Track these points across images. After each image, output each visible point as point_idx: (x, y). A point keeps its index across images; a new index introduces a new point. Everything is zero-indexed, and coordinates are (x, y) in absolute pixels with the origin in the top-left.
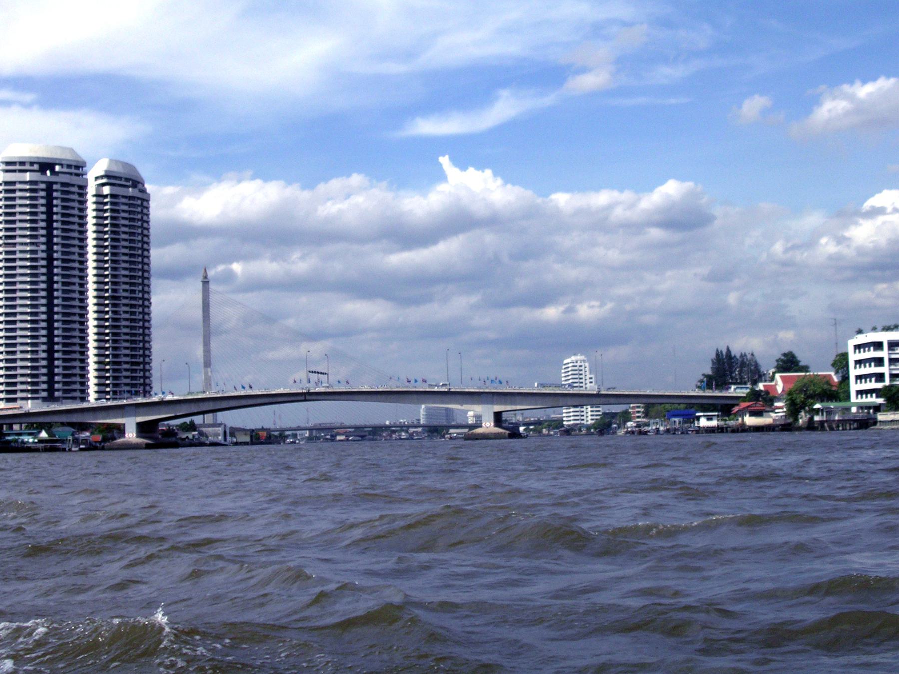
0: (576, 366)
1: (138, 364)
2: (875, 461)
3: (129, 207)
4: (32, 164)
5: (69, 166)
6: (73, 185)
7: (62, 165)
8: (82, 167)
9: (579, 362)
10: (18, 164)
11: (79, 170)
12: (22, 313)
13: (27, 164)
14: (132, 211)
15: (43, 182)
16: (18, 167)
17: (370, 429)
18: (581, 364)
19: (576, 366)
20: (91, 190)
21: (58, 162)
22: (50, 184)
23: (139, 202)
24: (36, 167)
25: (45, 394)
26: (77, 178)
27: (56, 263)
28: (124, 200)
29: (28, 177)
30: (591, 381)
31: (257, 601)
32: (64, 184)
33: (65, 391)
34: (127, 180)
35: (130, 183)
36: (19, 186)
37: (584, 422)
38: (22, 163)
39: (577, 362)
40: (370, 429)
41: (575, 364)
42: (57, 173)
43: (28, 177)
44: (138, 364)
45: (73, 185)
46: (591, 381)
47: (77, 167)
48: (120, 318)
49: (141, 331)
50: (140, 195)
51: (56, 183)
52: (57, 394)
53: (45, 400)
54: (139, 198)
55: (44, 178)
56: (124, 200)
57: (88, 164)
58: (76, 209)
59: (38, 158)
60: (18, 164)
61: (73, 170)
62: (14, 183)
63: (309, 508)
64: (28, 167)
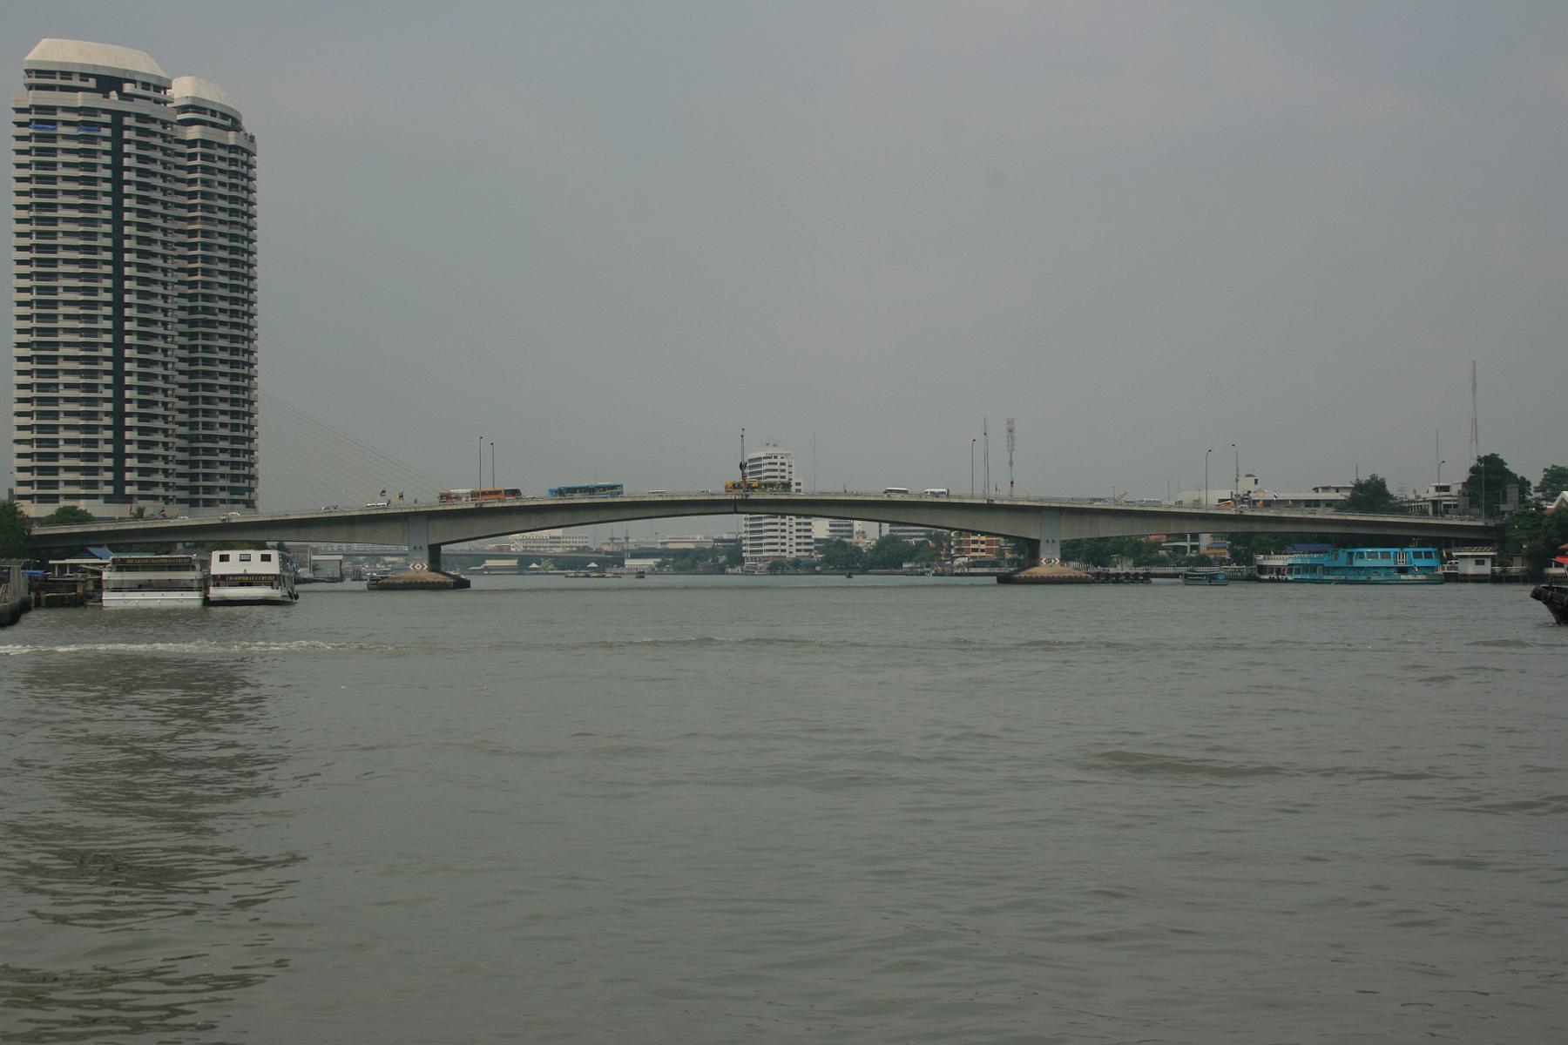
0: (776, 464)
4: (85, 76)
5: (146, 86)
6: (154, 120)
8: (165, 89)
9: (779, 457)
11: (160, 92)
12: (67, 344)
13: (74, 76)
15: (105, 111)
16: (58, 81)
18: (783, 461)
19: (776, 464)
22: (118, 115)
24: (92, 83)
25: (109, 490)
26: (157, 105)
27: (127, 257)
28: (221, 152)
29: (79, 99)
30: (798, 487)
31: (139, 833)
32: (141, 117)
33: (142, 485)
34: (224, 116)
37: (786, 554)
38: (66, 75)
39: (776, 457)
41: (773, 460)
42: (129, 97)
43: (79, 99)
45: (154, 120)
46: (798, 487)
47: (158, 89)
48: (214, 359)
50: (244, 145)
51: (128, 114)
52: (128, 490)
53: (108, 499)
55: (105, 104)
56: (221, 152)
58: (159, 163)
59: (95, 67)
60: (58, 76)
61: (151, 93)
62: (52, 109)
63: (258, 686)
64: (76, 82)
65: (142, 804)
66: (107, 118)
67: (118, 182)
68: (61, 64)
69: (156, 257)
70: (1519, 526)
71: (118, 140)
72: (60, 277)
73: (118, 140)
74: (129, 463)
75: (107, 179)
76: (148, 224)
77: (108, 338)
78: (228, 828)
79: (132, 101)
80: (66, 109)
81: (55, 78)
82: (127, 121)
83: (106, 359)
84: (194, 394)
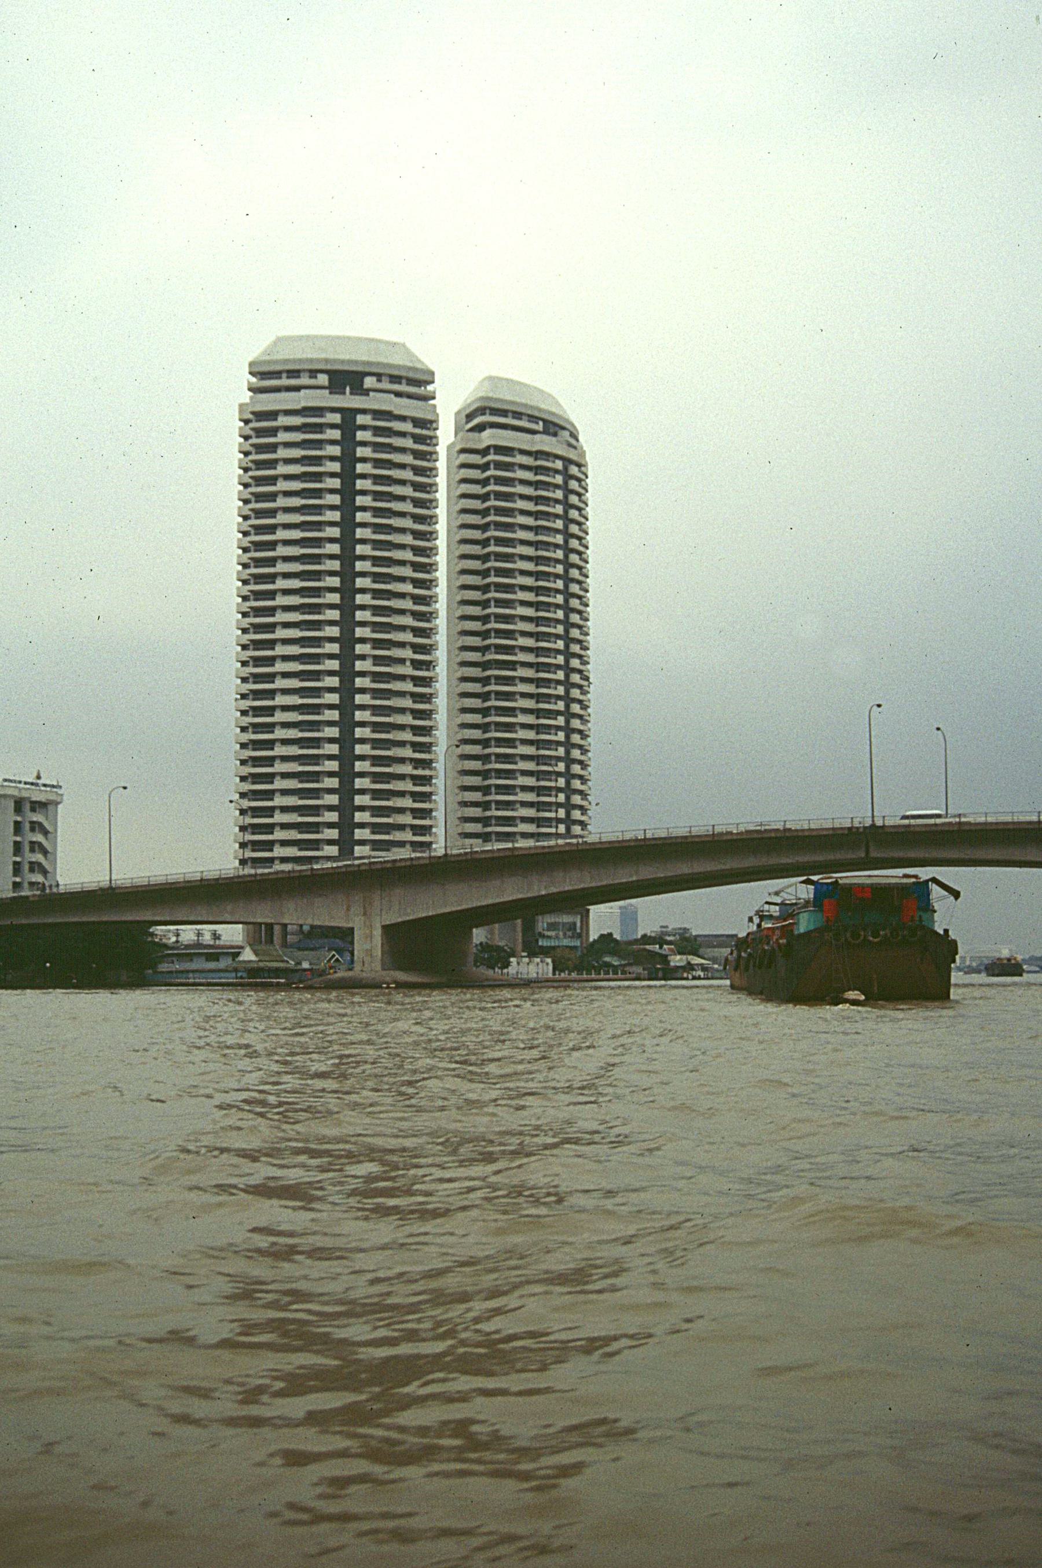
1: (554, 714)
2: (176, 1270)
3: (537, 687)
4: (313, 373)
6: (403, 418)
7: (379, 376)
10: (284, 375)
14: (543, 664)
15: (333, 410)
16: (285, 381)
17: (583, 1343)
20: (446, 435)
21: (367, 369)
22: (349, 414)
23: (559, 465)
24: (323, 379)
32: (378, 414)
35: (540, 427)
36: (283, 421)
38: (294, 373)
40: (583, 1343)
44: (554, 714)
47: (418, 383)
49: (562, 798)
51: (364, 411)
54: (557, 457)
57: (437, 378)
60: (284, 375)
62: (273, 415)
64: (305, 380)
65: (366, 1526)
66: (337, 418)
67: (347, 792)
68: (286, 361)
69: (404, 763)
70: (47, 968)
71: (348, 441)
72: (280, 513)
73: (348, 441)
74: (359, 783)
75: (335, 688)
76: (390, 790)
77: (333, 732)
78: (663, 1039)
79: (368, 395)
80: (288, 413)
81: (280, 378)
82: (361, 419)
83: (331, 825)
84: (487, 751)
